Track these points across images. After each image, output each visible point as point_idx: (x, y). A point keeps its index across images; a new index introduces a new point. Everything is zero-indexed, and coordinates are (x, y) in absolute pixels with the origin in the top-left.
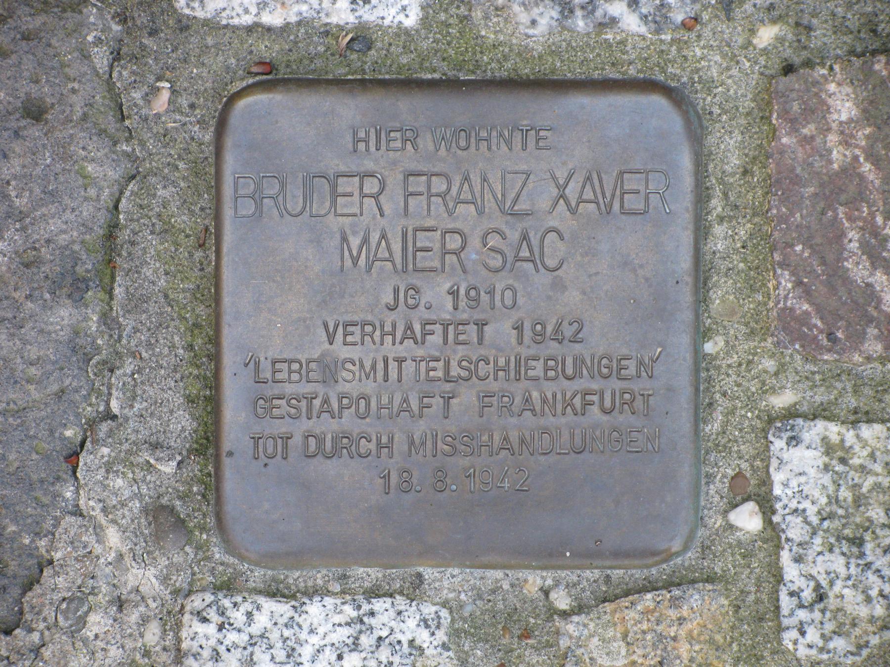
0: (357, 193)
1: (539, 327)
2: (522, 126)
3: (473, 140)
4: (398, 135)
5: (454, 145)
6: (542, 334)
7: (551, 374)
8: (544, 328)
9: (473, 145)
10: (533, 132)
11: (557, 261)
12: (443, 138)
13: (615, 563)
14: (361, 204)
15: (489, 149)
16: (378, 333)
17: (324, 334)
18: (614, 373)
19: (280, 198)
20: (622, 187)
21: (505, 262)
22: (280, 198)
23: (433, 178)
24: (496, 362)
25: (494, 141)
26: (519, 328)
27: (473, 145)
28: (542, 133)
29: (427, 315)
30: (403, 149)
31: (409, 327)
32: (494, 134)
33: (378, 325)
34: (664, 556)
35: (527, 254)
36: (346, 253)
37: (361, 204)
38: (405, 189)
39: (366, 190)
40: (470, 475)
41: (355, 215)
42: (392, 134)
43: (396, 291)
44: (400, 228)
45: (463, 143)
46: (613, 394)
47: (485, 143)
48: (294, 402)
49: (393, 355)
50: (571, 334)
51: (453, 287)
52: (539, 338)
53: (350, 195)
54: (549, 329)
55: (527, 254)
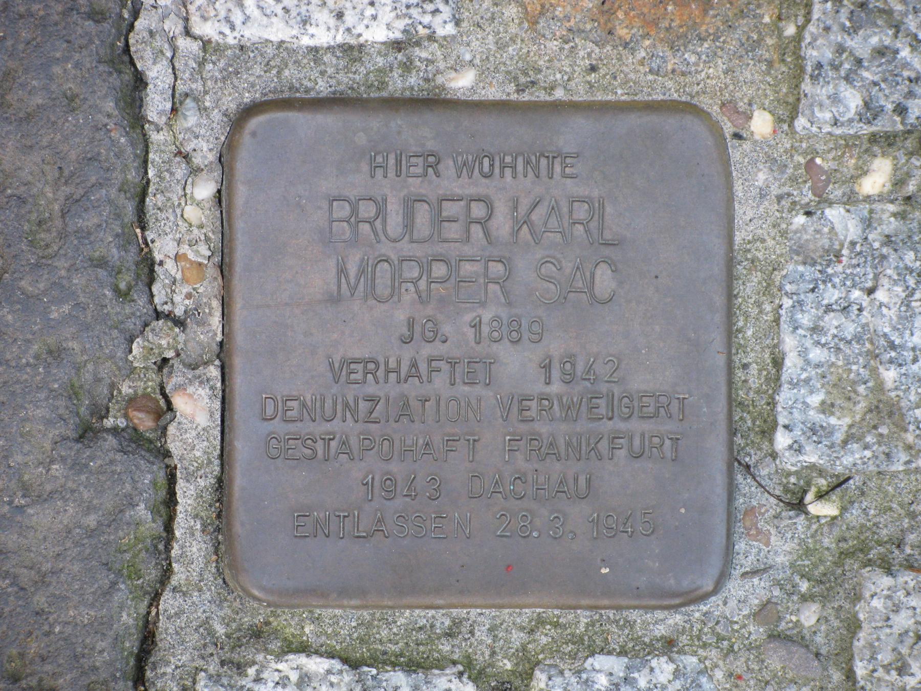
1: (568, 366)
2: (548, 152)
3: (497, 164)
4: (360, 367)
5: (476, 170)
6: (573, 375)
7: (656, 440)
8: (573, 365)
9: (497, 171)
10: (559, 159)
12: (465, 164)
16: (382, 367)
18: (636, 412)
19: (378, 224)
20: (357, 216)
22: (378, 224)
23: (473, 204)
25: (520, 168)
27: (497, 171)
28: (568, 160)
30: (425, 174)
31: (414, 365)
32: (520, 160)
36: (343, 280)
46: (643, 435)
48: (309, 442)
49: (414, 394)
50: (643, 387)
51: (475, 318)
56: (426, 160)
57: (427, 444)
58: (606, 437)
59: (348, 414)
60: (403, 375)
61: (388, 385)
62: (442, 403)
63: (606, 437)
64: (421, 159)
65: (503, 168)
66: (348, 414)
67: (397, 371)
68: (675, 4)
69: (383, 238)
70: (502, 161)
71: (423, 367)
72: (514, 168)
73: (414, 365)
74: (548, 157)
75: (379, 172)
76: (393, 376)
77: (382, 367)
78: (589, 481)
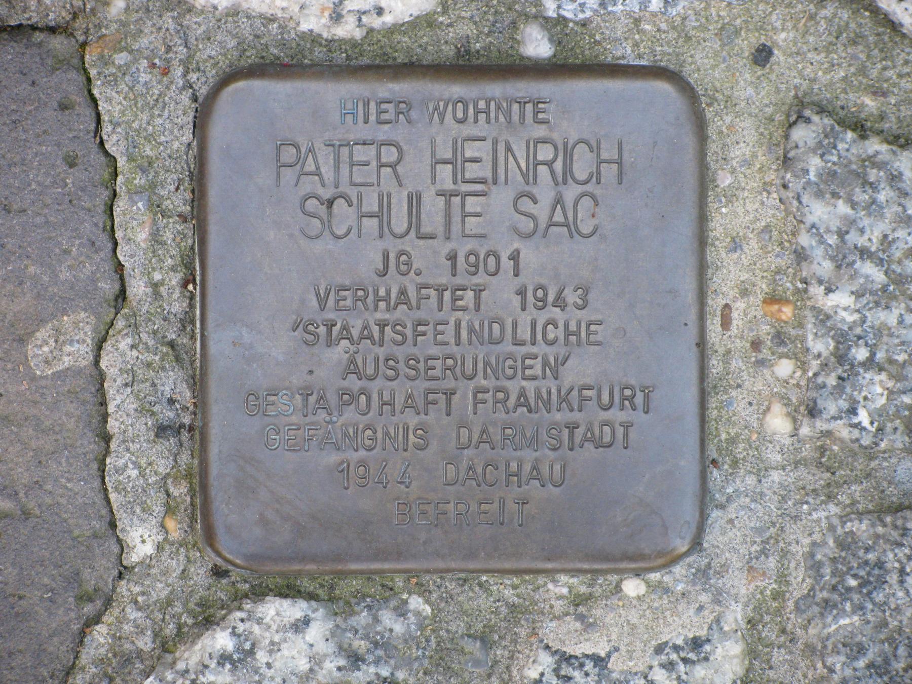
0: (374, 164)
3: (471, 111)
4: (390, 107)
8: (546, 295)
11: (591, 228)
13: (604, 566)
14: (379, 173)
15: (488, 122)
16: (371, 297)
17: (315, 299)
18: (519, 372)
21: (536, 226)
24: (566, 325)
26: (522, 292)
29: (419, 280)
31: (403, 292)
33: (371, 290)
34: (668, 558)
35: (562, 220)
37: (379, 173)
38: (278, 161)
39: (540, 157)
40: (343, 470)
41: (483, 181)
42: (384, 106)
43: (386, 257)
44: (406, 193)
45: (460, 115)
47: (484, 115)
52: (542, 303)
53: (367, 164)
54: (551, 298)
55: (562, 220)
56: (397, 106)
57: (322, 398)
58: (576, 389)
59: (474, 337)
60: (414, 303)
61: (442, 313)
62: (539, 329)
63: (576, 389)
64: (391, 105)
65: (477, 112)
66: (474, 337)
67: (387, 298)
68: (910, 417)
69: (575, 233)
70: (476, 106)
71: (412, 293)
72: (487, 113)
73: (403, 292)
74: (519, 102)
75: (349, 118)
76: (382, 305)
77: (371, 297)
78: (564, 468)
